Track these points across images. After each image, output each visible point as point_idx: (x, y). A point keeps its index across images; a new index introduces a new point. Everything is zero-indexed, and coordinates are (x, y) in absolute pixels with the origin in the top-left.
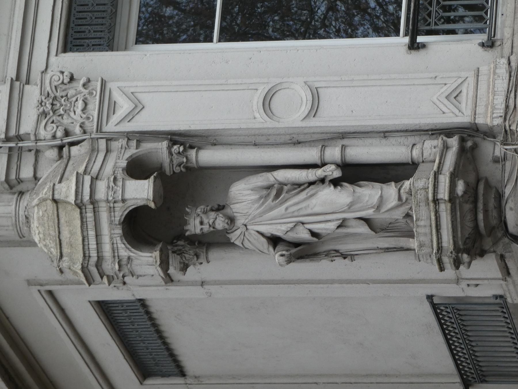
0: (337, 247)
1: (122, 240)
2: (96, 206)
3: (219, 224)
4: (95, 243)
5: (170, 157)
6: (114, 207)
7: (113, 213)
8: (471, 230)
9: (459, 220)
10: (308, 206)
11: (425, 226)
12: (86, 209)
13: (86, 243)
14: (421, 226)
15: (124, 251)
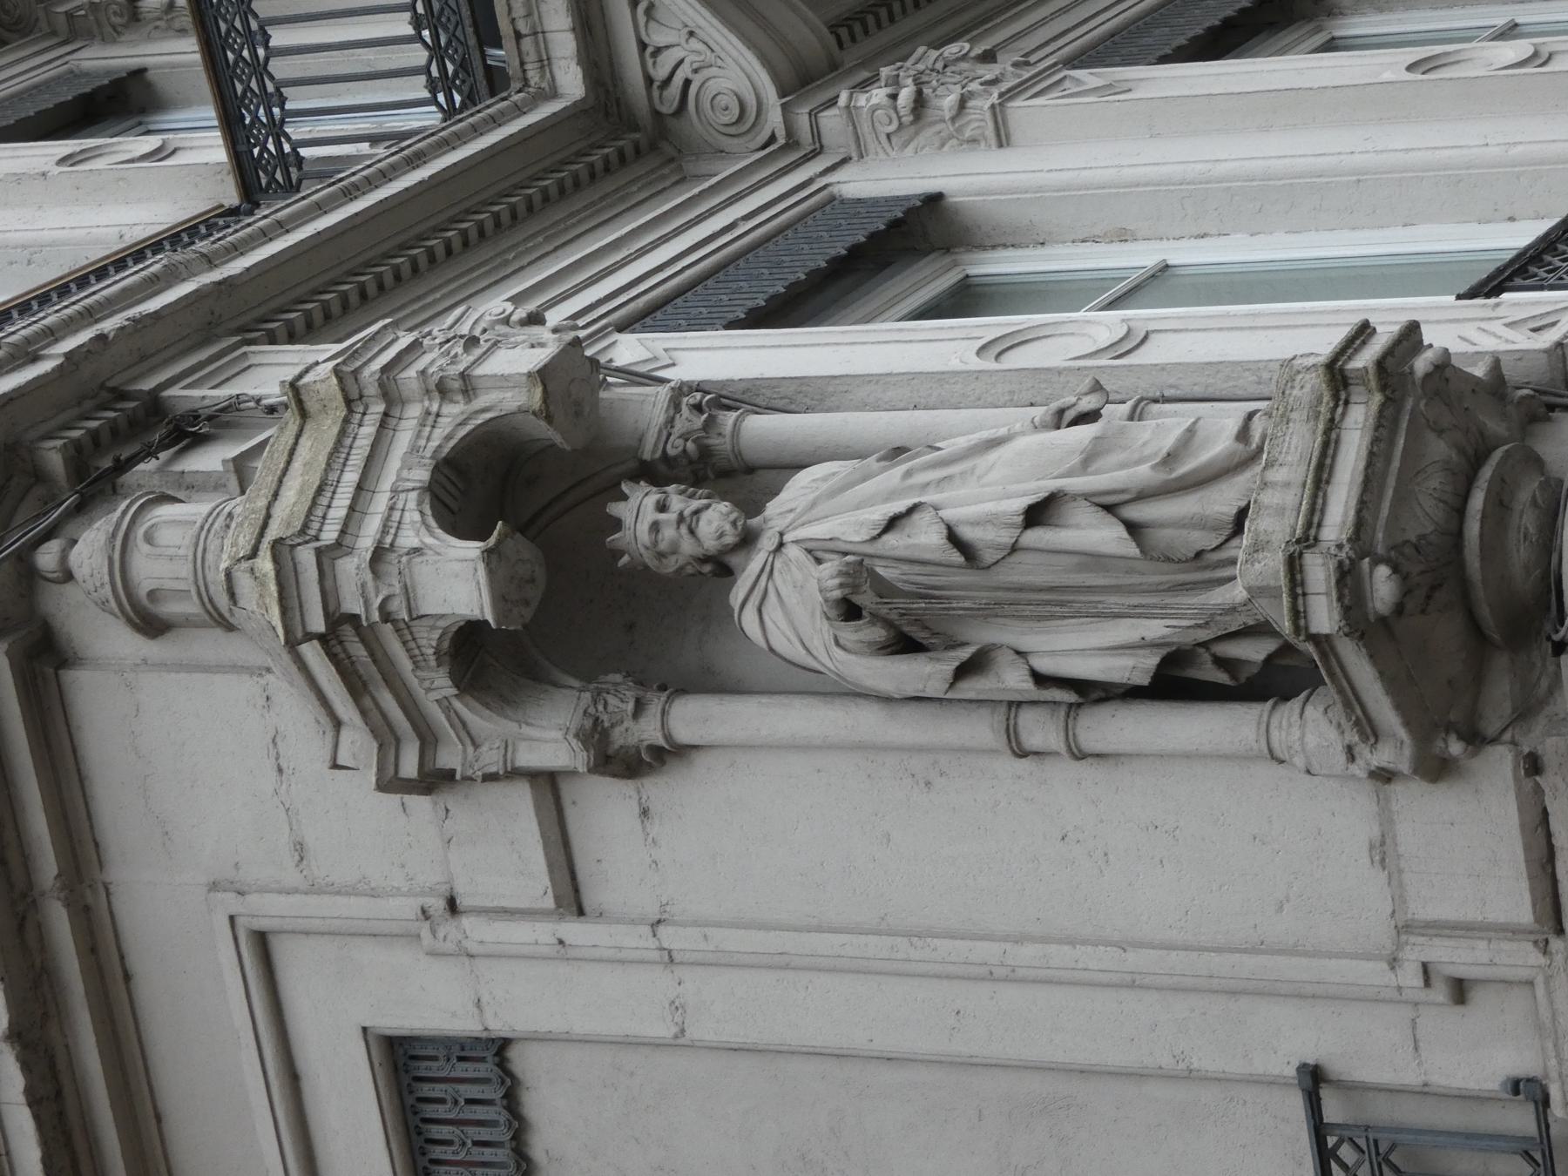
0: (1027, 642)
1: (420, 503)
2: (396, 412)
3: (710, 522)
4: (348, 502)
5: (672, 412)
6: (438, 415)
7: (428, 429)
8: (1430, 528)
9: (1396, 464)
10: (973, 469)
11: (1287, 485)
12: (364, 414)
13: (324, 501)
14: (1274, 484)
15: (413, 511)
